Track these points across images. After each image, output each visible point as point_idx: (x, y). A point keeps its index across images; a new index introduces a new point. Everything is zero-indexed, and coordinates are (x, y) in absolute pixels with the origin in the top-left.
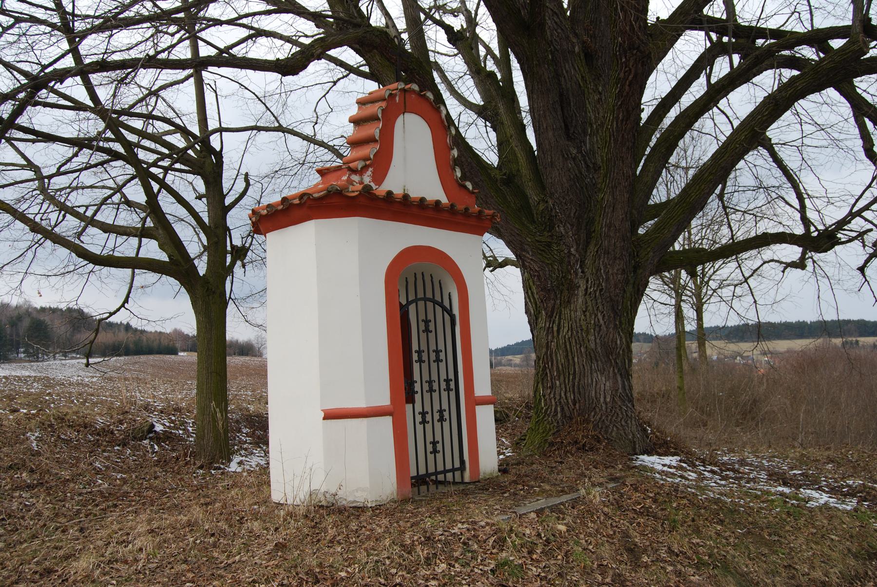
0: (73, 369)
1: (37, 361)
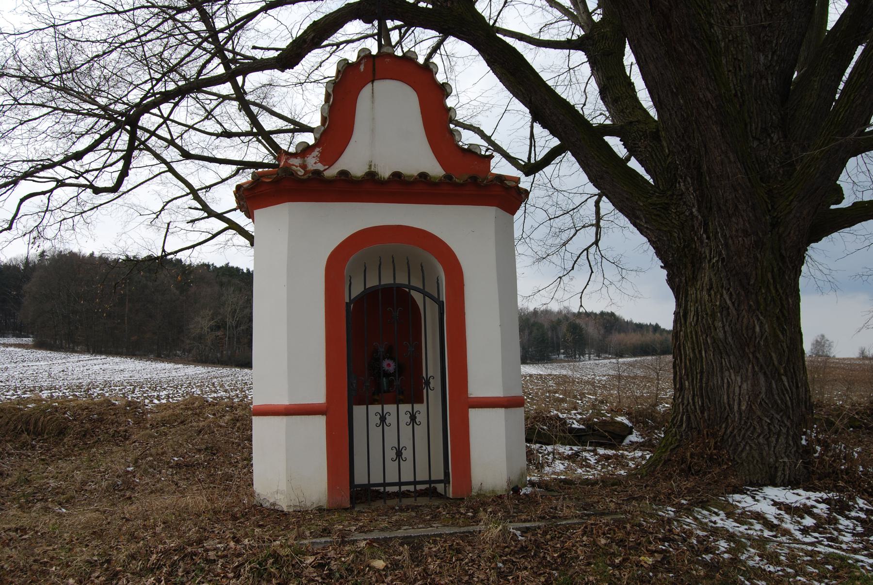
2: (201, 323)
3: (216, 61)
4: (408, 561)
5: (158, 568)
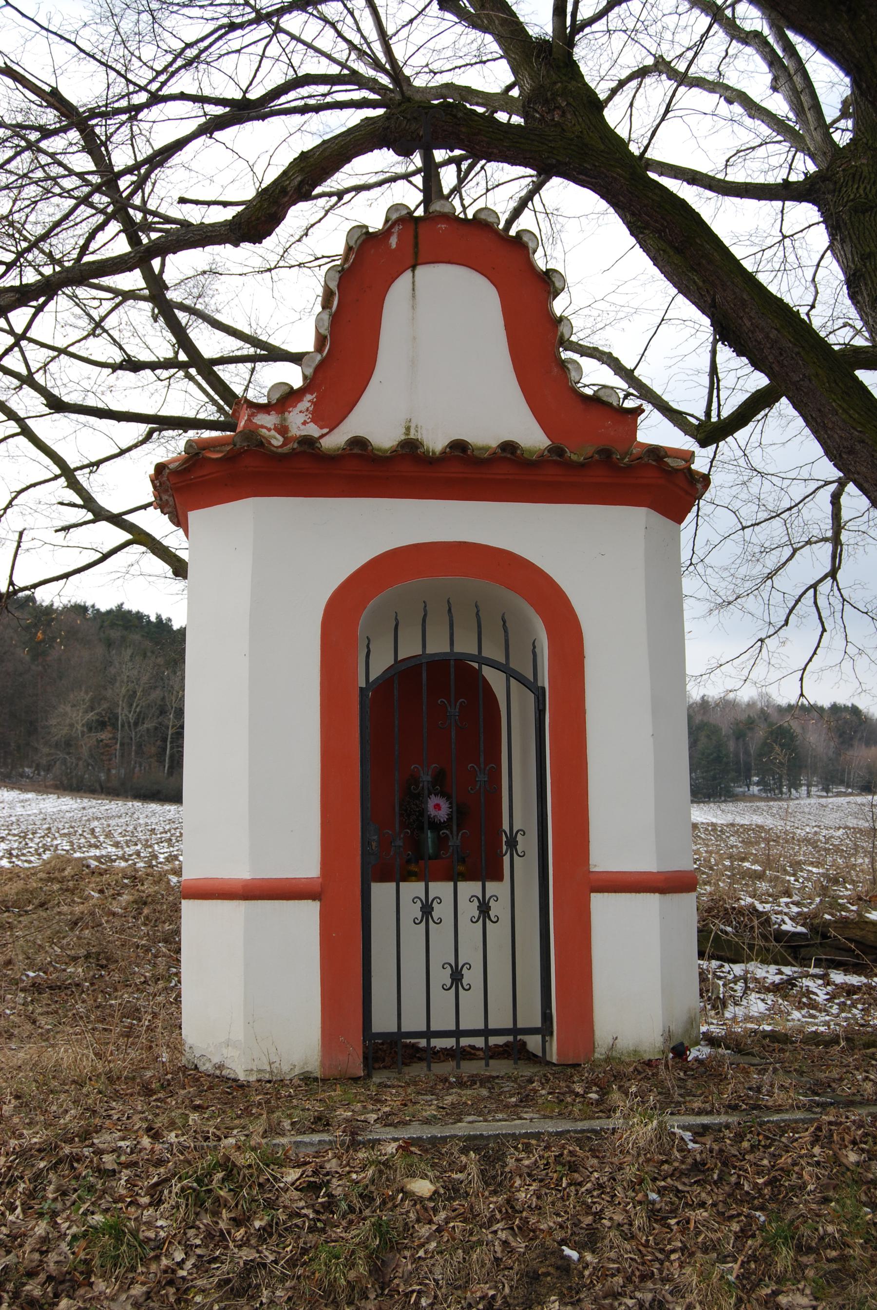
0: (838, 815)
1: (780, 799)
2: (70, 716)
3: (114, 226)
4: (477, 1184)
5: (9, 1183)
